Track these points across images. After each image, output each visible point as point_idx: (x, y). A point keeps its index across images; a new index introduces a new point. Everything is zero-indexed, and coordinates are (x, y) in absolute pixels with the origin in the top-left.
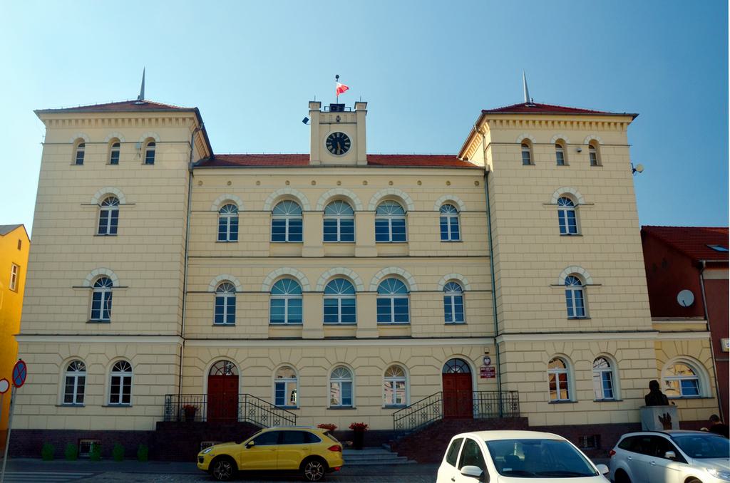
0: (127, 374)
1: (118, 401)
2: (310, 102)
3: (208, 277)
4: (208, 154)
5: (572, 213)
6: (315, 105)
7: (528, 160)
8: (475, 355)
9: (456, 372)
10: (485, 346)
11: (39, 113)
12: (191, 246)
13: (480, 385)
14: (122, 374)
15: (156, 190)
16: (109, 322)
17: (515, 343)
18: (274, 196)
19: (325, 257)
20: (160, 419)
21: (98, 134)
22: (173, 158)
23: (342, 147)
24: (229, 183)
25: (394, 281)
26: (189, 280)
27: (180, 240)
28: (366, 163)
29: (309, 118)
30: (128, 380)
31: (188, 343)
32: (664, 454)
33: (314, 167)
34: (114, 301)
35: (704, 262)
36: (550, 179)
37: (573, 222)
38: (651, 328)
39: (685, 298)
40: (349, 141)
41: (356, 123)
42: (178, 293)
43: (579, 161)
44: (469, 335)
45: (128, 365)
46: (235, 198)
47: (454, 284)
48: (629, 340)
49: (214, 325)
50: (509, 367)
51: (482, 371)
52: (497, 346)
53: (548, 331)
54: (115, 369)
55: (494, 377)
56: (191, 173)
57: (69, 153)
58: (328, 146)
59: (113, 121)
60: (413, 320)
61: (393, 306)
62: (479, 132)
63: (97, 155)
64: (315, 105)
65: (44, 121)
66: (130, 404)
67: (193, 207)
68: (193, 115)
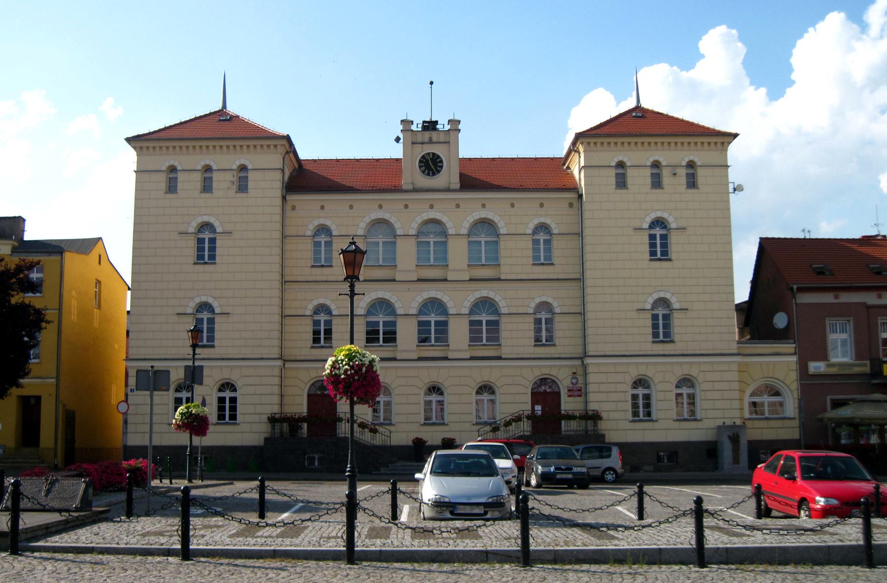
0: (233, 395)
1: (224, 419)
2: (402, 121)
3: (306, 301)
4: (296, 166)
5: (664, 237)
6: (406, 123)
7: (621, 183)
8: (563, 377)
9: (545, 391)
10: (573, 366)
11: (129, 140)
12: (287, 271)
13: (568, 404)
14: (228, 394)
15: (253, 214)
16: (213, 346)
17: (598, 364)
18: (367, 220)
19: (419, 280)
20: (266, 435)
21: (190, 161)
22: (268, 185)
23: (436, 166)
24: (322, 207)
25: (485, 304)
26: (286, 304)
27: (277, 268)
28: (458, 186)
29: (401, 136)
30: (233, 400)
31: (288, 365)
32: (538, 404)
33: (406, 191)
34: (217, 327)
35: (795, 287)
36: (642, 203)
37: (664, 246)
38: (736, 351)
39: (780, 320)
40: (441, 161)
41: (449, 143)
42: (277, 318)
43: (674, 184)
44: (557, 356)
45: (233, 385)
46: (328, 223)
47: (545, 306)
48: (712, 363)
49: (312, 347)
50: (591, 388)
51: (569, 390)
52: (585, 367)
53: (632, 353)
54: (220, 390)
55: (580, 396)
56: (284, 198)
57: (161, 180)
58: (420, 167)
59: (204, 148)
60: (503, 342)
61: (433, 328)
62: (576, 151)
63: (189, 183)
64: (406, 123)
65: (135, 148)
66: (238, 421)
67: (289, 231)
68: (284, 142)
